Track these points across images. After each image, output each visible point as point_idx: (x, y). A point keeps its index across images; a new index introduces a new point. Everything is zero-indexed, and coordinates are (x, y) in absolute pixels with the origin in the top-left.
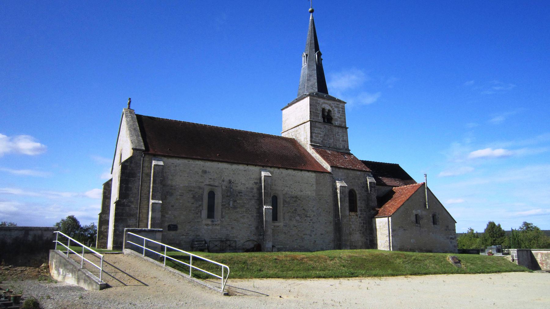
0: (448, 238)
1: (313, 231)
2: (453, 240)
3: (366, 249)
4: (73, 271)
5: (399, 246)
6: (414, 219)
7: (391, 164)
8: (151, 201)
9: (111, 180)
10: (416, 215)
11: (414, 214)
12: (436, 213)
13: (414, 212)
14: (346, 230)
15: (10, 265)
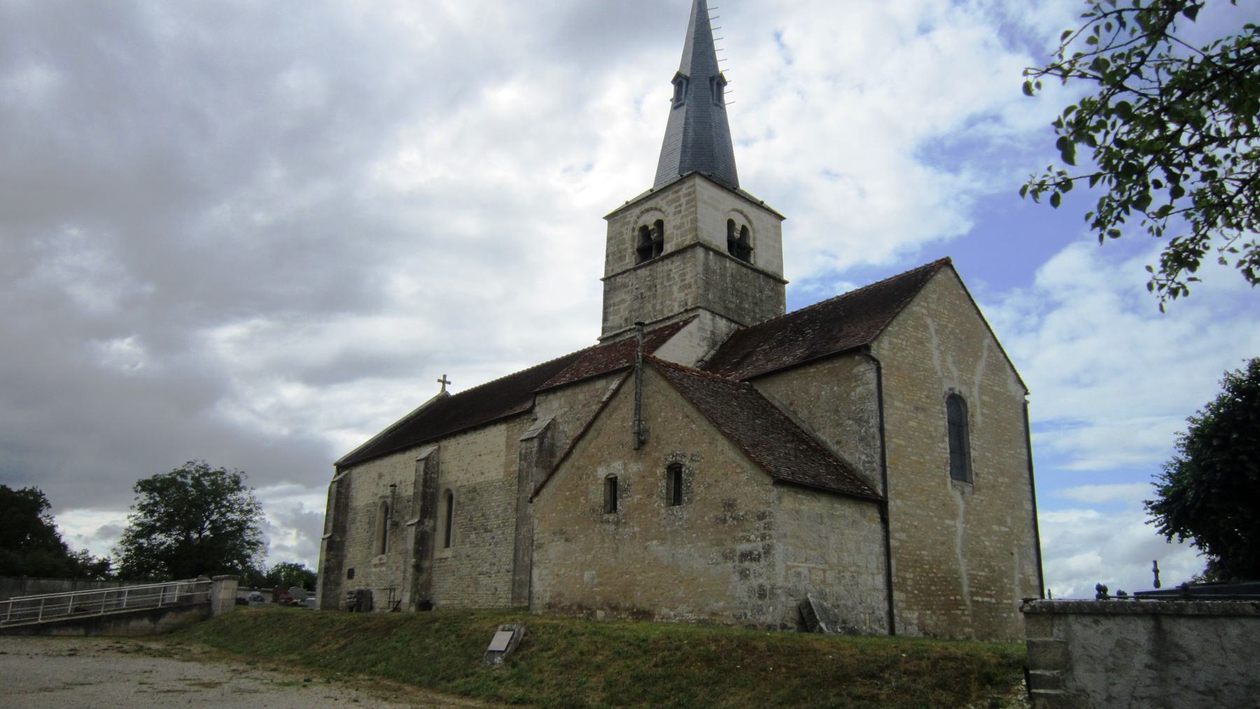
0: (726, 557)
1: (494, 564)
2: (753, 566)
3: (175, 579)
4: (360, 671)
5: (548, 594)
6: (598, 494)
7: (514, 374)
8: (40, 621)
9: (1091, 186)
10: (612, 482)
11: (599, 482)
12: (684, 456)
13: (602, 472)
14: (523, 558)
15: (31, 501)
